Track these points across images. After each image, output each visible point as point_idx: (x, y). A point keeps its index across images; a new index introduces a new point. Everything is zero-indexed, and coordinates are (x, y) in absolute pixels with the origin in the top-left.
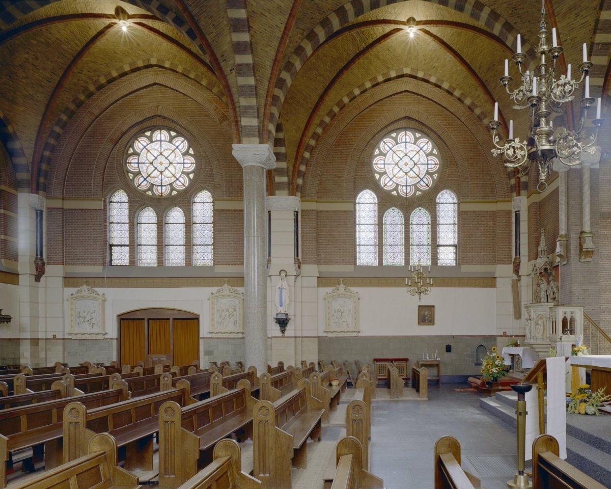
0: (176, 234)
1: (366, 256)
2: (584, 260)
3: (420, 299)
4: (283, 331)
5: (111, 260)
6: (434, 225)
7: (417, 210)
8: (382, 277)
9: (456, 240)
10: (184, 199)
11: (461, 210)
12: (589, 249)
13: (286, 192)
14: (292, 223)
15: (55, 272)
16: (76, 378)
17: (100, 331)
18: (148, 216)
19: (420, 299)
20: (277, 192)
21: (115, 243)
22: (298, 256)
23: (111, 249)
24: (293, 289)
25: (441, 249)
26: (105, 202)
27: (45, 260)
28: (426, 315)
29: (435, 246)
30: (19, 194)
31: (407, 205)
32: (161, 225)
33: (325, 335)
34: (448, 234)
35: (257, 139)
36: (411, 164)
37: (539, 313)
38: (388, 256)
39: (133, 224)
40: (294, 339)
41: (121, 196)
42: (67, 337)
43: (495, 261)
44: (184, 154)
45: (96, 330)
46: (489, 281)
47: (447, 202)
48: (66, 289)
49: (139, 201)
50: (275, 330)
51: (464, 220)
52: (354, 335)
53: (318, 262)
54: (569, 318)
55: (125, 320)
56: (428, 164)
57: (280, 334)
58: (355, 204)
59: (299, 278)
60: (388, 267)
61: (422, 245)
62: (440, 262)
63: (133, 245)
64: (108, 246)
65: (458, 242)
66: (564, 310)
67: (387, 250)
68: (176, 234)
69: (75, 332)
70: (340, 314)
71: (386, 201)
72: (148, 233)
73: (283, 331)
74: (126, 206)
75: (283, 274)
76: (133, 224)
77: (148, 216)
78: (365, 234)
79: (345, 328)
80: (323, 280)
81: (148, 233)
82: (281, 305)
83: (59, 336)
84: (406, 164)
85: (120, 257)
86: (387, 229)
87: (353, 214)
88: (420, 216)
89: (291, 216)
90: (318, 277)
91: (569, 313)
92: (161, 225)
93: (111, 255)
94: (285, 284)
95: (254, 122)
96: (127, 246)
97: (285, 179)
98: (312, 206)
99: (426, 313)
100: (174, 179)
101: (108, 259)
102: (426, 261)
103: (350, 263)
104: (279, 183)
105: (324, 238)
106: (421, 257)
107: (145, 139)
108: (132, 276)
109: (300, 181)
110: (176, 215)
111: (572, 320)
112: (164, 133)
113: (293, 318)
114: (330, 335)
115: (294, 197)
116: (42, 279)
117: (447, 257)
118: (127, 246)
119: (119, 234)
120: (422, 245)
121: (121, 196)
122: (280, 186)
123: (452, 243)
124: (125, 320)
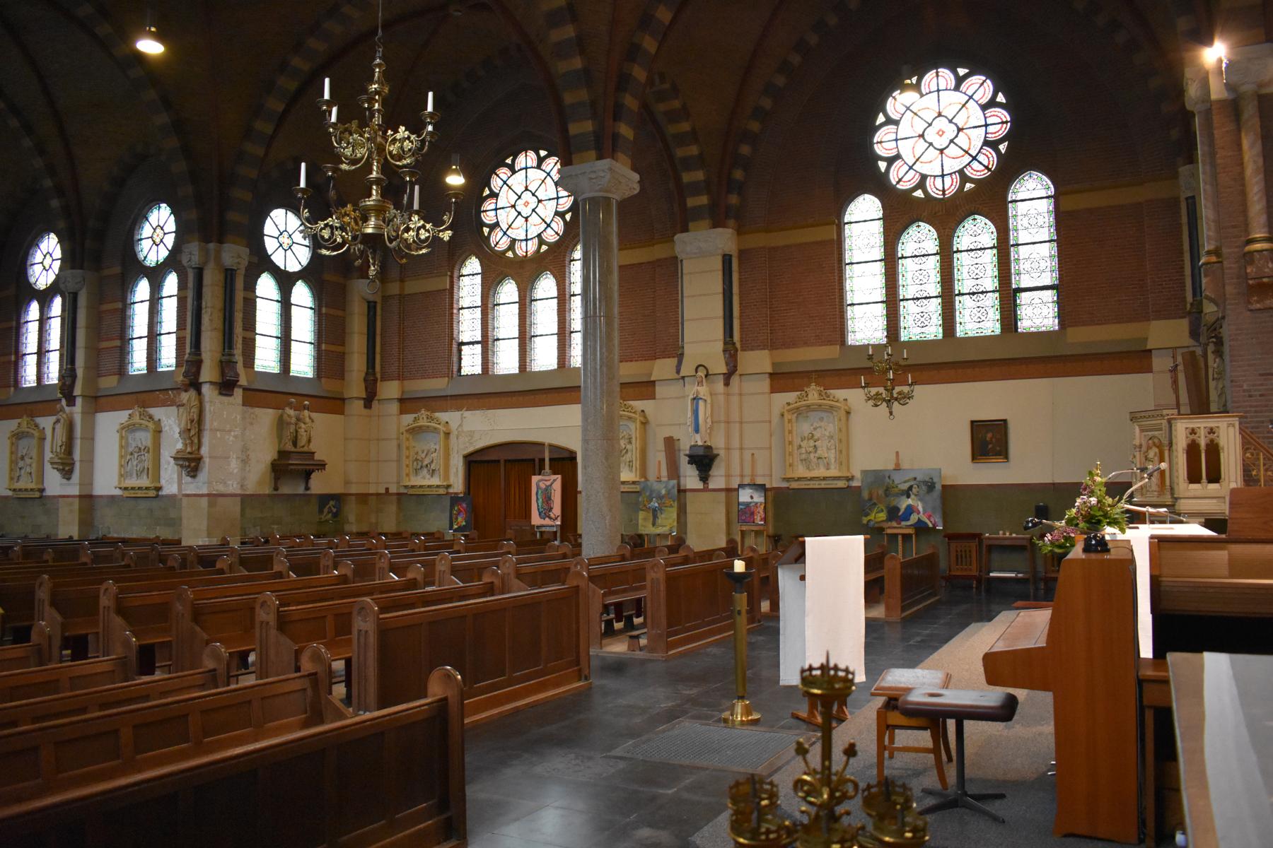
0: (975, 269)
1: (865, 326)
2: (1258, 306)
3: (891, 413)
4: (704, 478)
5: (460, 368)
6: (1004, 248)
7: (969, 223)
8: (900, 368)
9: (1056, 274)
10: (989, 197)
11: (1062, 209)
12: (1265, 280)
13: (707, 222)
14: (719, 277)
15: (390, 389)
16: (454, 559)
17: (33, 486)
18: (508, 291)
19: (891, 413)
20: (691, 225)
21: (465, 340)
22: (731, 336)
23: (460, 351)
24: (721, 398)
25: (1024, 298)
26: (452, 277)
27: (738, 345)
28: (989, 440)
29: (1009, 296)
30: (730, 230)
31: (946, 215)
32: (946, 254)
33: (785, 485)
34: (1037, 261)
35: (593, 154)
36: (951, 131)
37: (1150, 433)
38: (967, 319)
39: (487, 307)
40: (723, 494)
41: (473, 265)
42: (403, 491)
43: (1143, 315)
44: (984, 107)
45: (435, 481)
46: (1135, 359)
47: (1033, 200)
48: (777, 396)
49: (901, 211)
50: (691, 478)
51: (1070, 230)
52: (841, 484)
53: (772, 345)
54: (1203, 443)
55: (474, 462)
56: (986, 125)
57: (700, 485)
58: (840, 226)
59: (735, 380)
60: (911, 344)
61: (982, 292)
62: (960, 332)
63: (487, 342)
64: (455, 346)
65: (1061, 278)
66: (1191, 426)
67: (909, 312)
68: (975, 269)
69: (796, 475)
70: (812, 443)
71: (901, 211)
72: (920, 275)
73: (704, 478)
74: (478, 279)
75: (701, 373)
76: (487, 307)
77: (508, 291)
78: (863, 283)
79: (821, 472)
80: (781, 379)
81: (920, 275)
82: (697, 431)
83: (393, 490)
84: (941, 133)
85: (471, 362)
86: (907, 269)
87: (837, 245)
88: (976, 233)
89: (718, 264)
90: (771, 374)
91: (1202, 433)
92: (946, 254)
93: (460, 359)
94: (703, 390)
95: (588, 126)
96: (477, 342)
97: (703, 200)
98: (758, 240)
99: (989, 436)
100: (967, 159)
101: (455, 369)
102: (934, 331)
103: (830, 342)
104: (695, 208)
105: (790, 298)
106: (978, 319)
107: (505, 170)
108: (494, 393)
109: (734, 199)
110: (546, 286)
111: (1214, 450)
112: (945, 73)
113: (722, 453)
114: (794, 485)
115: (720, 230)
116: (375, 404)
117: (1038, 314)
118: (477, 342)
119: (468, 326)
120: (982, 292)
121: (473, 265)
122: (696, 214)
123: (1048, 282)
124: (474, 462)
